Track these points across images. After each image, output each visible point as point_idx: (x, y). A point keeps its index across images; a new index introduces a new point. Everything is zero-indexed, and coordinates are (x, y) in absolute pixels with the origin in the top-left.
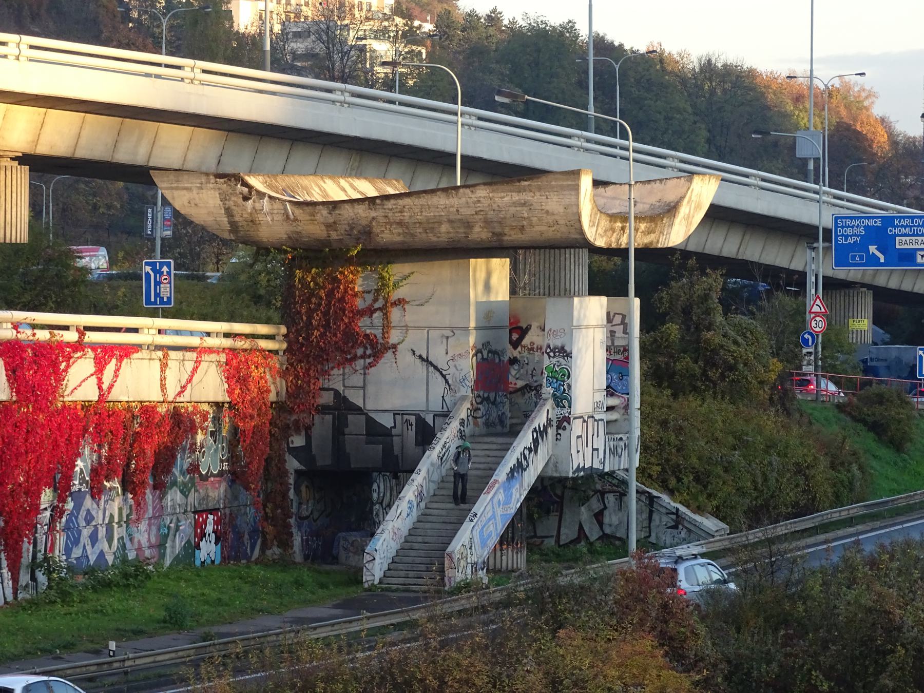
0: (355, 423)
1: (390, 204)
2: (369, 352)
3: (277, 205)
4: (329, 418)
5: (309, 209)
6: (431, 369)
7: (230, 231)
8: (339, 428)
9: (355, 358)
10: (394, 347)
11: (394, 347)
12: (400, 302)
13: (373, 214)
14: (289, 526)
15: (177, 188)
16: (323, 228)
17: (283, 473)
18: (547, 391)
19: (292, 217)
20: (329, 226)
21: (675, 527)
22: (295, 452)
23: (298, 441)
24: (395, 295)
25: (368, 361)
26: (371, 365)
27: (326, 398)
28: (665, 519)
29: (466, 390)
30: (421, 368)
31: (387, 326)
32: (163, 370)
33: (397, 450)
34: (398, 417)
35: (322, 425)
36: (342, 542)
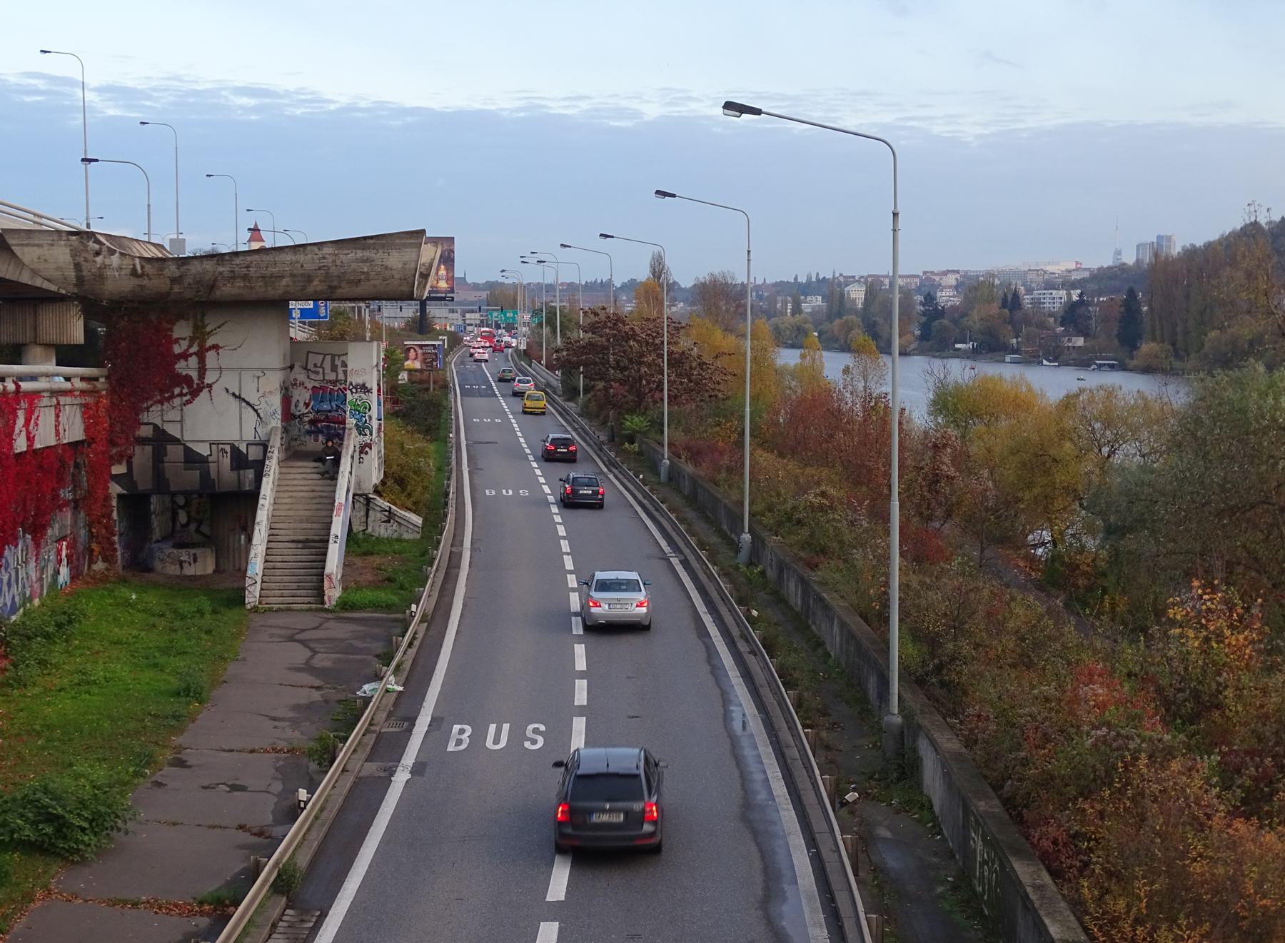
0: (174, 452)
1: (238, 261)
2: (185, 391)
3: (127, 261)
4: (149, 449)
5: (157, 265)
6: (244, 404)
7: (75, 285)
8: (158, 457)
9: (173, 397)
10: (210, 386)
11: (210, 386)
12: (216, 347)
13: (220, 269)
14: (113, 543)
15: (27, 245)
16: (168, 281)
17: (107, 498)
18: (351, 422)
19: (140, 271)
20: (174, 280)
21: (388, 521)
22: (117, 478)
23: (119, 469)
24: (209, 343)
25: (185, 399)
26: (189, 402)
27: (145, 431)
28: (379, 515)
29: (277, 422)
30: (235, 404)
31: (202, 370)
32: (57, 416)
33: (213, 475)
34: (214, 447)
35: (142, 456)
36: (157, 554)
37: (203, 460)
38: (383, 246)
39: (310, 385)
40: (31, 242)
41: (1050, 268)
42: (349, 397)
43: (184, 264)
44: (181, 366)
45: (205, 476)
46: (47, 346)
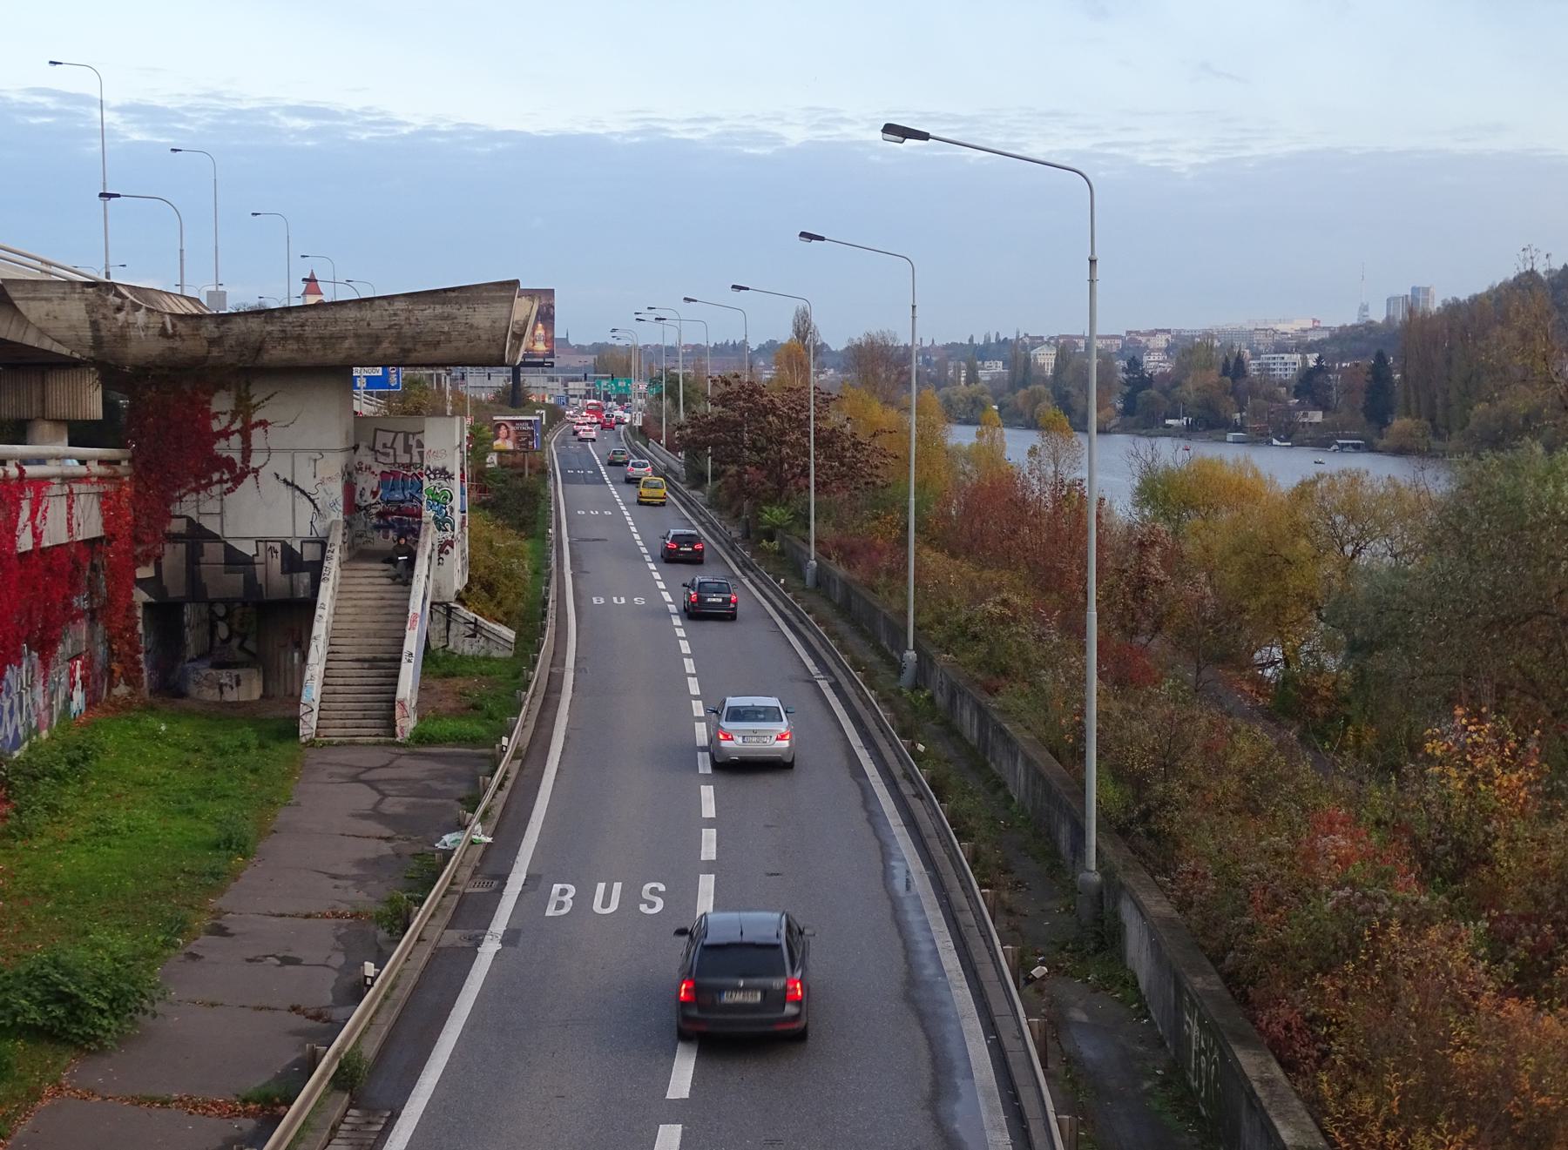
0: (212, 552)
1: (290, 318)
2: (226, 477)
3: (155, 318)
4: (181, 547)
5: (191, 323)
6: (297, 493)
7: (92, 348)
8: (193, 558)
9: (211, 484)
10: (256, 471)
11: (256, 471)
12: (263, 423)
13: (269, 328)
14: (138, 662)
15: (33, 299)
16: (205, 343)
17: (131, 607)
18: (428, 514)
19: (170, 331)
20: (212, 342)
21: (474, 636)
22: (143, 583)
23: (145, 572)
24: (255, 418)
25: (226, 486)
26: (230, 490)
27: (177, 526)
28: (462, 628)
29: (337, 515)
30: (286, 492)
31: (247, 452)
32: (70, 507)
33: (260, 579)
34: (261, 545)
35: (173, 556)
36: (192, 676)
37: (248, 561)
38: (467, 300)
39: (378, 469)
40: (38, 295)
41: (1281, 327)
42: (426, 484)
43: (224, 322)
44: (220, 447)
45: (250, 580)
46: (58, 421)
